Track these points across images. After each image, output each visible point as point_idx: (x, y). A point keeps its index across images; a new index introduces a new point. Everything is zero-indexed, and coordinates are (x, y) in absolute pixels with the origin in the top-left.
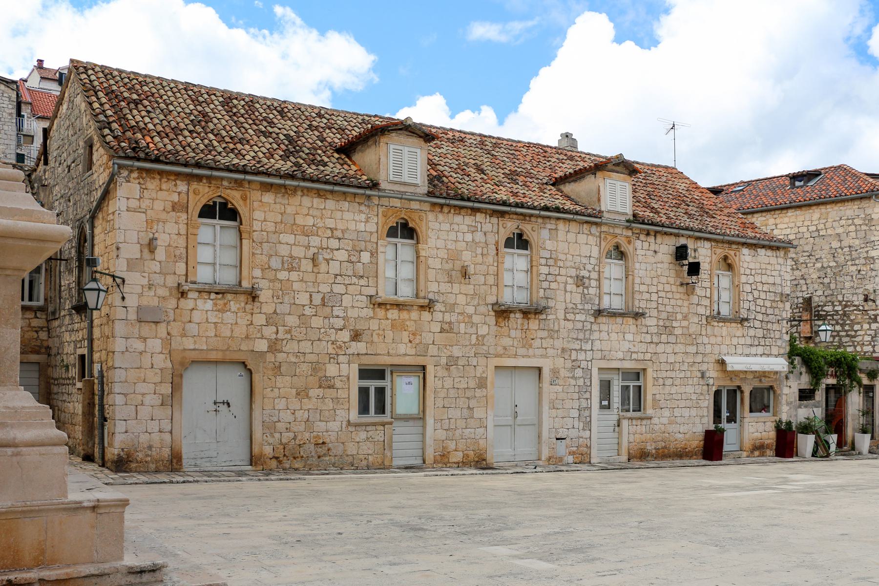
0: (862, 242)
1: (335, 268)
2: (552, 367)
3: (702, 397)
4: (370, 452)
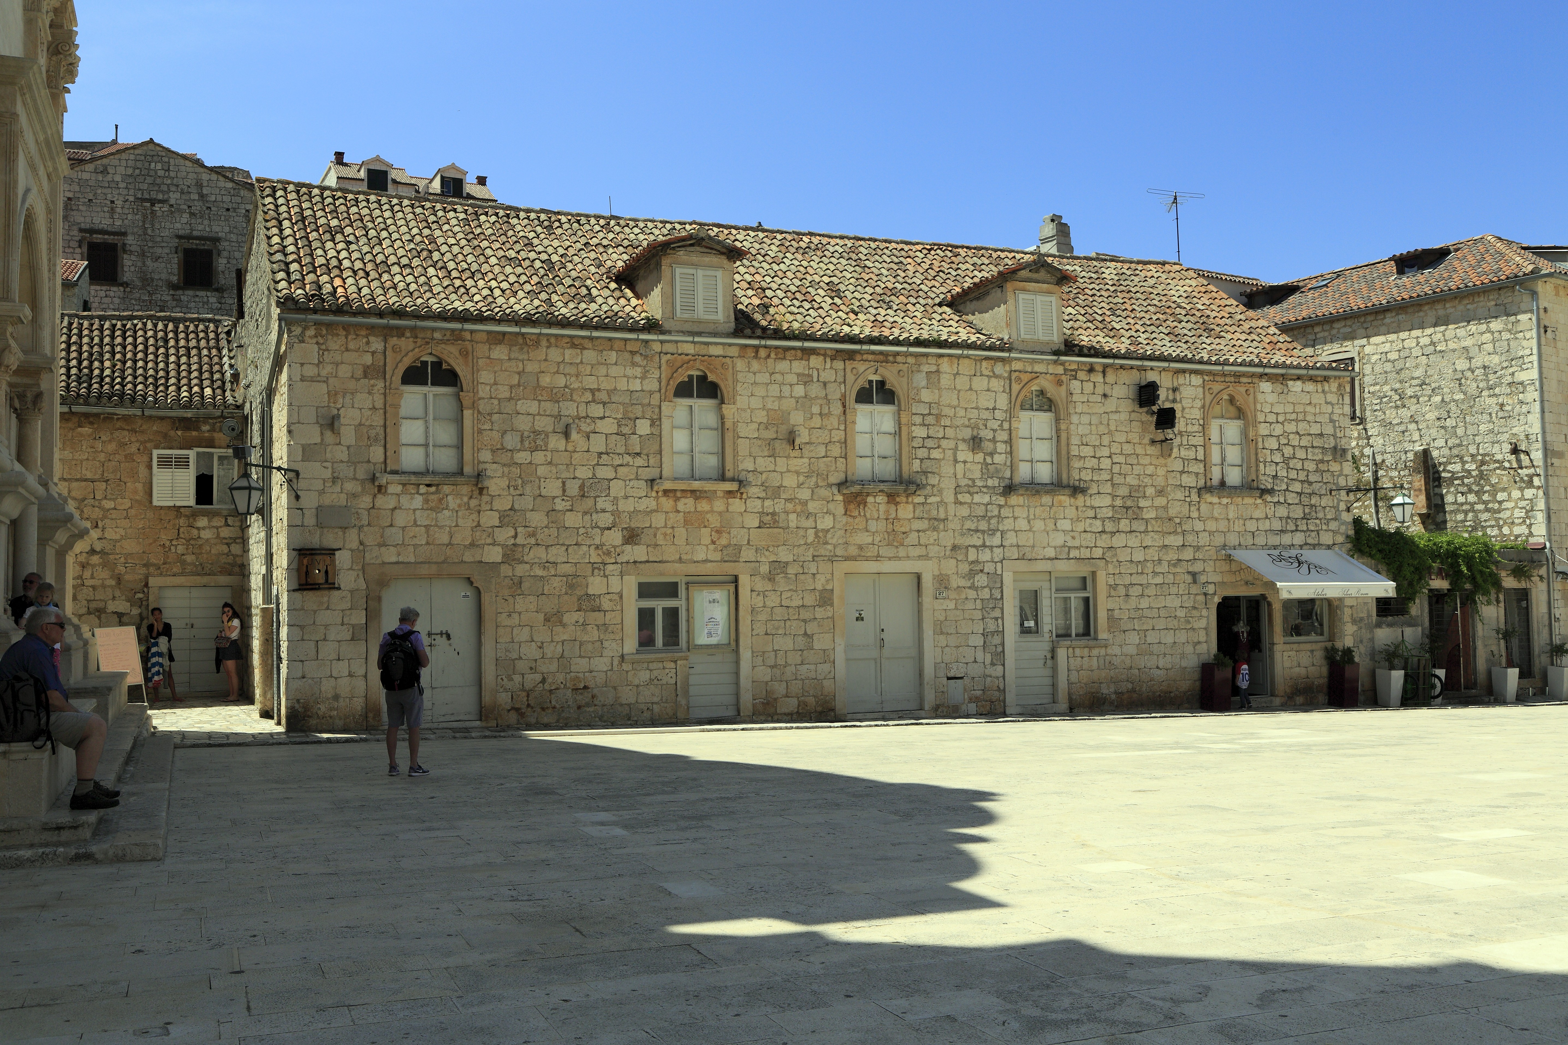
0: (1504, 358)
1: (598, 444)
2: (937, 573)
3: (1195, 613)
4: (656, 699)
